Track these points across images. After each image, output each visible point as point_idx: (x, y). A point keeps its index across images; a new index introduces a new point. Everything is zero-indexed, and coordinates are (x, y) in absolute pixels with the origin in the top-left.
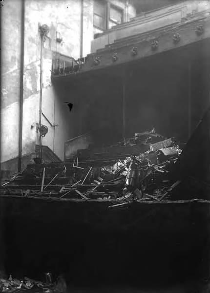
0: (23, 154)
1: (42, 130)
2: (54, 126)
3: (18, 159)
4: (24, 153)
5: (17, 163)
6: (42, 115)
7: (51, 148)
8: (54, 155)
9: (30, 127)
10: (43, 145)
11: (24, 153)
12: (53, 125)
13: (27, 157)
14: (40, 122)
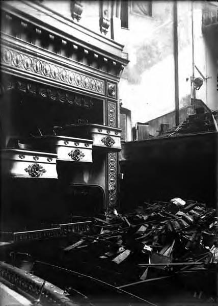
1: (198, 83)
2: (206, 79)
3: (175, 114)
4: (181, 106)
5: (174, 117)
6: (195, 68)
7: (205, 102)
8: (208, 108)
10: (197, 98)
11: (181, 106)
13: (185, 110)
14: (193, 75)
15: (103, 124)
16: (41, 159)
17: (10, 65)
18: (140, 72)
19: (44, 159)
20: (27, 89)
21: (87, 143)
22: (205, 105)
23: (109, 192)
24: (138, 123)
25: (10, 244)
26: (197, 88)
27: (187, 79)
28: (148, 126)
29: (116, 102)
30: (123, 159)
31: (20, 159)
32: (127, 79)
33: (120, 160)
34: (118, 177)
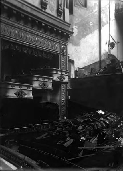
0: (102, 59)
1: (112, 45)
2: (117, 43)
7: (116, 56)
9: (105, 43)
10: (112, 54)
11: (102, 58)
12: (116, 42)
13: (104, 61)
15: (58, 68)
16: (24, 88)
17: (6, 35)
18: (80, 39)
19: (25, 88)
20: (16, 48)
21: (49, 79)
22: (116, 58)
23: (61, 107)
24: (78, 68)
25: (4, 136)
26: (112, 48)
27: (106, 43)
28: (84, 69)
29: (66, 56)
30: (70, 88)
31: (12, 88)
32: (72, 43)
33: (68, 88)
34: (67, 98)
